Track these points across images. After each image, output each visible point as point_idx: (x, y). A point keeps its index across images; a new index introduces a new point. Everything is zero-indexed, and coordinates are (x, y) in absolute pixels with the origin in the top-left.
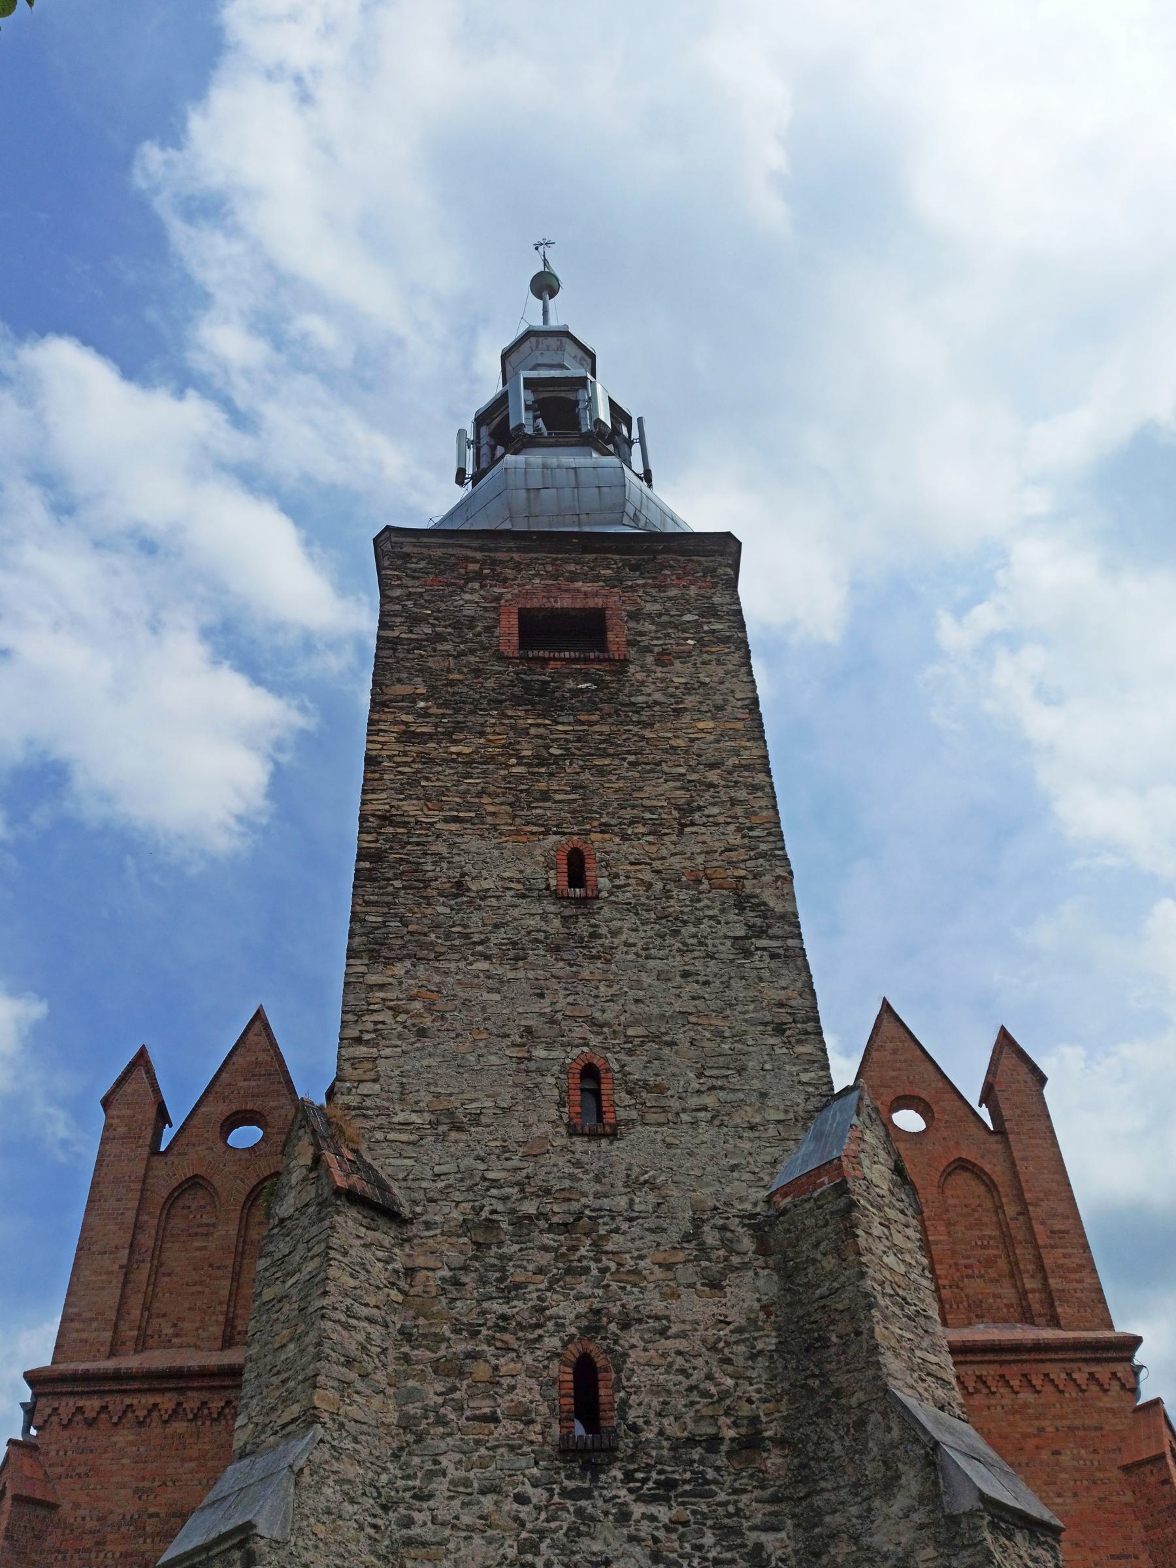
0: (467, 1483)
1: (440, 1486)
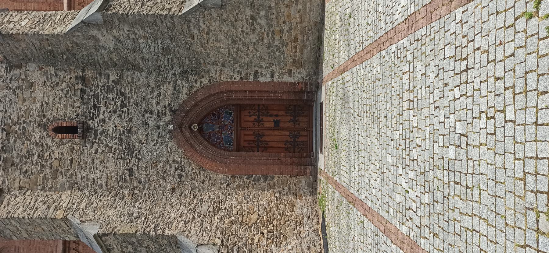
0: (90, 168)
1: (91, 176)
